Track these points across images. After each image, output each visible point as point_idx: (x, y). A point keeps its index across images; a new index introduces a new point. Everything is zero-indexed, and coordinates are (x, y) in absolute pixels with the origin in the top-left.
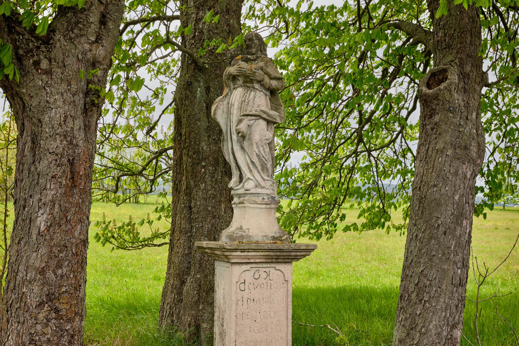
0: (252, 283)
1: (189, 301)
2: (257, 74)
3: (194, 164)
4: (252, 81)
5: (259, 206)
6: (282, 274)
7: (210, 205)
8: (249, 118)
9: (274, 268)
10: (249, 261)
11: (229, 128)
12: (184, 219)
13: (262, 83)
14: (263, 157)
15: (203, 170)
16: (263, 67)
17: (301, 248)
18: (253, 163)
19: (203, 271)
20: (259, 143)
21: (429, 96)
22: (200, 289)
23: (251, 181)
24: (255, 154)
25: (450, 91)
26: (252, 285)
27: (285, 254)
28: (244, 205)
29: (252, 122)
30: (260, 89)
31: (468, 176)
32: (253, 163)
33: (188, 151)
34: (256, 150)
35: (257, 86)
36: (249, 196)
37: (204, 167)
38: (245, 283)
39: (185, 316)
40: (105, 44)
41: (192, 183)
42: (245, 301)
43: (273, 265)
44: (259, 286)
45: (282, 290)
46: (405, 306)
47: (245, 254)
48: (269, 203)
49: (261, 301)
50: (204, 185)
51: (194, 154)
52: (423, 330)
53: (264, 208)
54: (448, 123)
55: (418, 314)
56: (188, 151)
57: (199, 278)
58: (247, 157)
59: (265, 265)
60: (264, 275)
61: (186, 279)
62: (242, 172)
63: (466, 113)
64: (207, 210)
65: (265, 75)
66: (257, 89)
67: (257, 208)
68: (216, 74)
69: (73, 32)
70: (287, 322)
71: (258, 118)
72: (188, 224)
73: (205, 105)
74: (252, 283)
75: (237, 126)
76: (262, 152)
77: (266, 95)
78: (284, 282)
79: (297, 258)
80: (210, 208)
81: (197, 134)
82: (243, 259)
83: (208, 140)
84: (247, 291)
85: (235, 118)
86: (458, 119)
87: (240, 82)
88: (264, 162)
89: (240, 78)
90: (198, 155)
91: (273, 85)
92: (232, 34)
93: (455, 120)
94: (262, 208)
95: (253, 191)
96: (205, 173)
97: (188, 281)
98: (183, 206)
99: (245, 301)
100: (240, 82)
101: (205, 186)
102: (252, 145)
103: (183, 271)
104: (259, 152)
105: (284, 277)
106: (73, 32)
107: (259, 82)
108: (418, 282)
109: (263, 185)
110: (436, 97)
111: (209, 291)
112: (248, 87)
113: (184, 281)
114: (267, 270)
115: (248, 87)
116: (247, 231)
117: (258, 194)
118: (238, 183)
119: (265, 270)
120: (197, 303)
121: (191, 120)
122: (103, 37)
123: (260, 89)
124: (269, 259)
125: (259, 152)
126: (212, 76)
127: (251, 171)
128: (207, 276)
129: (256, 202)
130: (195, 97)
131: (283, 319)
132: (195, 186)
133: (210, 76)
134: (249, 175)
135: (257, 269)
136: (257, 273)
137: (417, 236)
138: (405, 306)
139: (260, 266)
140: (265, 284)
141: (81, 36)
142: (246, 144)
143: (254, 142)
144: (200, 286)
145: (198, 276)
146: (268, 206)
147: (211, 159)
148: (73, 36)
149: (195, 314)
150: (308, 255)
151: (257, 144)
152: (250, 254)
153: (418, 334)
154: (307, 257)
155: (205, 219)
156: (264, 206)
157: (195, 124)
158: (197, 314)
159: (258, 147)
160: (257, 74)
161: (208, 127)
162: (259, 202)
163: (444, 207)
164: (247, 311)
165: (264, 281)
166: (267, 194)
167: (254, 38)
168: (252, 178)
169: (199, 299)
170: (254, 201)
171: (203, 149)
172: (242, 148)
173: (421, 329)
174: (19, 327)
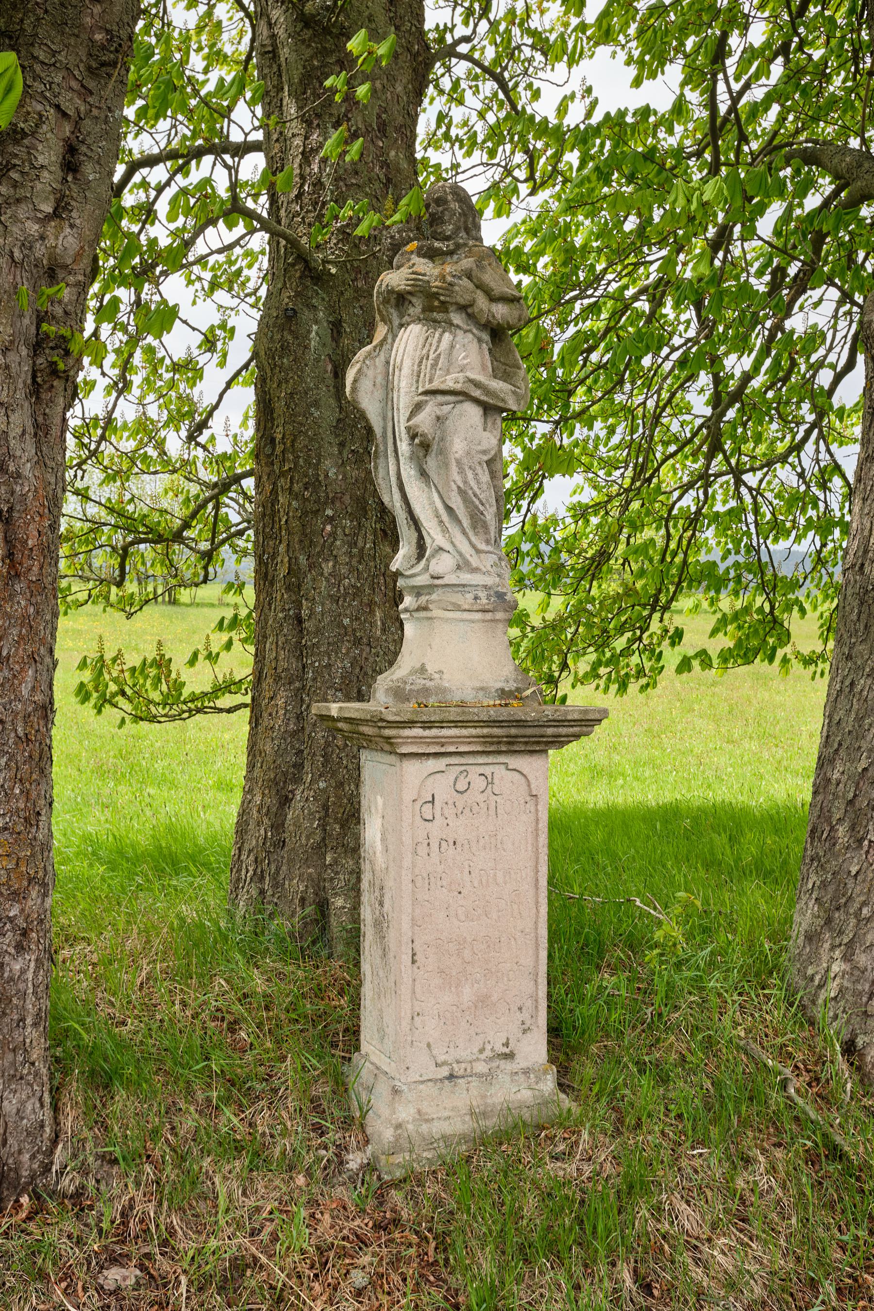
0: (450, 802)
1: (301, 846)
2: (457, 288)
3: (305, 513)
4: (444, 307)
5: (466, 615)
6: (523, 780)
7: (348, 612)
8: (440, 398)
9: (503, 767)
10: (443, 750)
12: (284, 648)
13: (470, 310)
14: (475, 495)
15: (328, 528)
16: (471, 270)
17: (569, 717)
19: (334, 774)
22: (327, 815)
23: (445, 555)
24: (454, 487)
26: (451, 806)
29: (447, 408)
30: (465, 327)
33: (292, 483)
35: (457, 318)
36: (440, 591)
37: (330, 519)
39: (291, 880)
40: (78, 221)
41: (302, 559)
43: (502, 759)
44: (467, 810)
45: (524, 818)
46: (821, 854)
47: (434, 732)
50: (331, 564)
51: (306, 489)
53: (478, 621)
55: (853, 873)
56: (292, 483)
57: (324, 790)
58: (435, 496)
59: (481, 760)
60: (481, 783)
61: (292, 792)
64: (340, 625)
65: (479, 292)
66: (458, 326)
67: (463, 620)
68: (357, 290)
71: (461, 398)
72: (293, 660)
73: (329, 367)
74: (450, 802)
76: (473, 483)
77: (480, 340)
78: (528, 798)
80: (346, 622)
81: (311, 440)
82: (429, 744)
83: (340, 453)
85: (404, 400)
87: (416, 309)
88: (477, 507)
90: (315, 491)
91: (499, 317)
92: (395, 186)
96: (333, 534)
97: (298, 797)
98: (281, 615)
101: (334, 566)
102: (447, 465)
103: (285, 774)
104: (465, 482)
105: (529, 786)
107: (463, 308)
108: (855, 796)
111: (347, 820)
112: (435, 321)
113: (287, 797)
114: (487, 770)
115: (435, 321)
116: (437, 676)
117: (464, 586)
119: (481, 770)
120: (320, 848)
121: (296, 405)
122: (73, 203)
123: (465, 327)
125: (465, 482)
126: (347, 295)
128: (342, 784)
129: (459, 606)
130: (306, 347)
131: (527, 887)
132: (311, 567)
133: (342, 293)
136: (462, 777)
137: (852, 684)
138: (821, 854)
139: (471, 760)
140: (482, 805)
141: (18, 201)
142: (431, 464)
144: (326, 808)
145: (322, 785)
146: (489, 616)
147: (347, 499)
149: (315, 876)
150: (587, 734)
151: (458, 462)
153: (853, 921)
155: (335, 646)
156: (478, 616)
157: (307, 414)
158: (319, 874)
159: (461, 471)
160: (457, 288)
161: (339, 421)
162: (467, 607)
164: (440, 869)
165: (481, 798)
166: (485, 587)
167: (450, 197)
168: (447, 546)
169: (324, 839)
170: (453, 604)
171: (327, 476)
172: (423, 474)
173: (860, 909)
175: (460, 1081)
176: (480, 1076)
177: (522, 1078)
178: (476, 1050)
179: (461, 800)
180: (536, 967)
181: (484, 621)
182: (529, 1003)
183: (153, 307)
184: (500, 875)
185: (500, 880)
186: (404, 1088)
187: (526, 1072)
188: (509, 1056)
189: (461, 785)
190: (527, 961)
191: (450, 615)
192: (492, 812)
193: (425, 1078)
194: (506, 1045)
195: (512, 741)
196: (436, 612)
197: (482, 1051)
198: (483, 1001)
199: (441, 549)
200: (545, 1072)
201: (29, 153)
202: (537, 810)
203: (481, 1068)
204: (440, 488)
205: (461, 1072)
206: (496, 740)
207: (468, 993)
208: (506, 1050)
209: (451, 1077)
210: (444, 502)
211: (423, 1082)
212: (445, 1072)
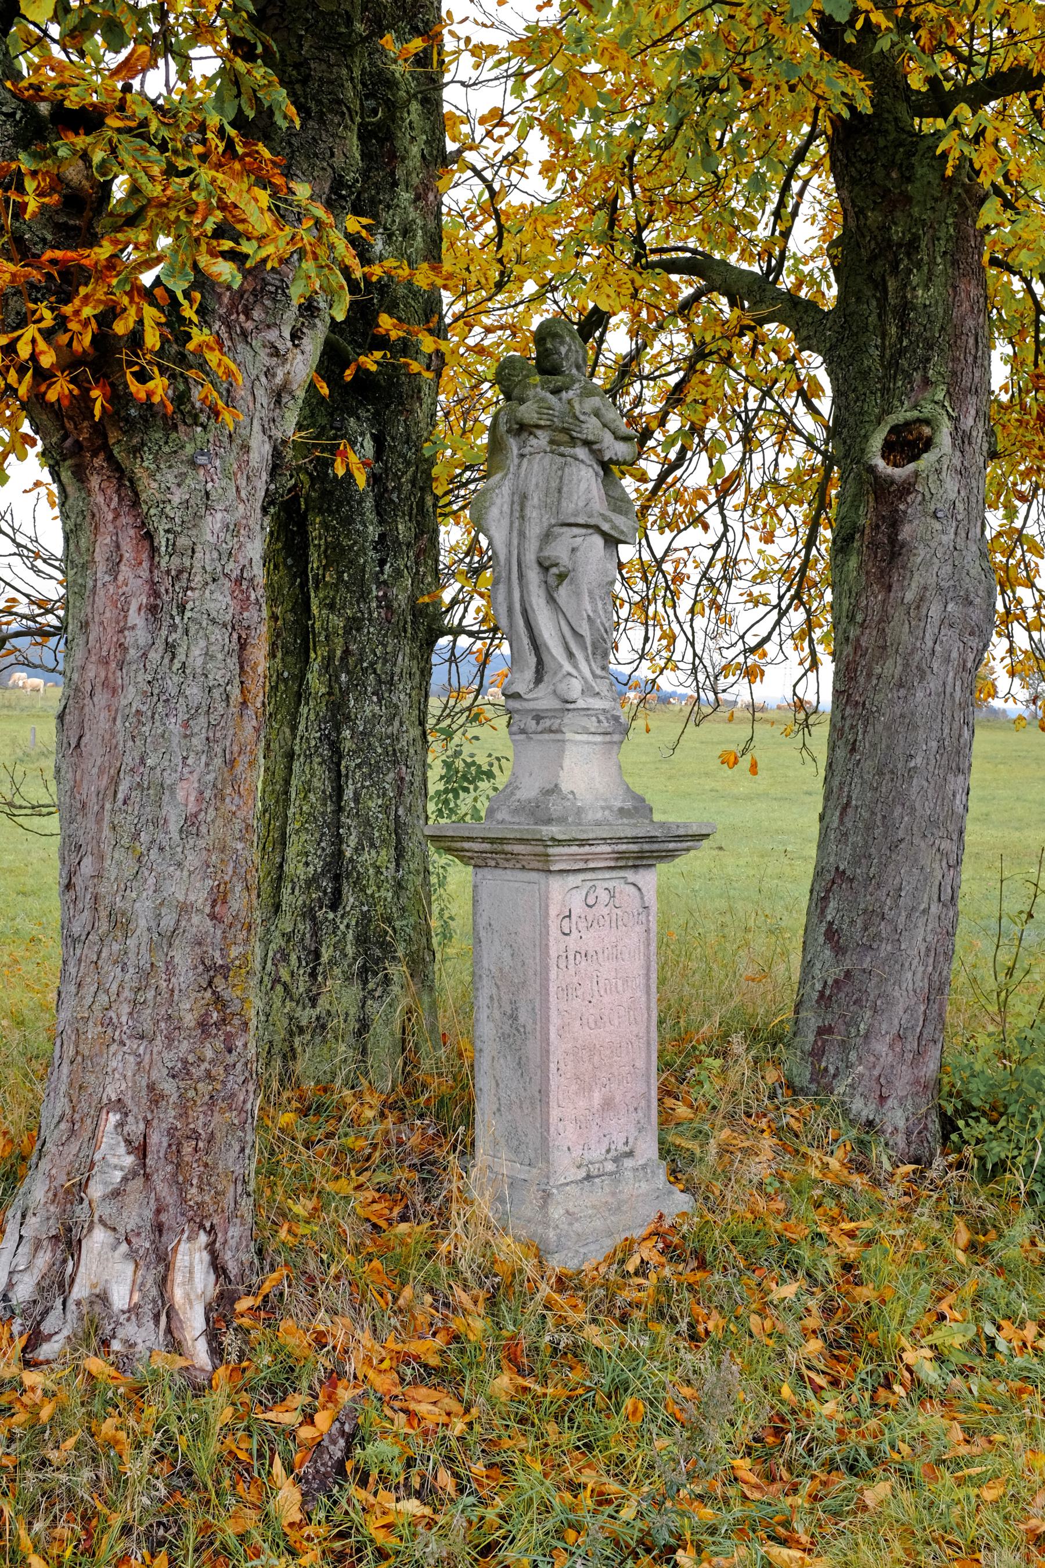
4: (573, 441)
5: (591, 738)
6: (637, 893)
8: (576, 531)
11: (515, 552)
13: (595, 447)
18: (575, 633)
20: (597, 591)
21: (892, 483)
25: (938, 472)
27: (655, 847)
28: (558, 736)
29: (579, 540)
30: (588, 462)
31: (969, 665)
32: (575, 633)
34: (589, 608)
35: (581, 452)
36: (570, 715)
38: (569, 916)
42: (571, 957)
44: (595, 924)
45: (638, 928)
47: (587, 849)
48: (609, 730)
49: (600, 955)
52: (879, 1003)
54: (933, 544)
58: (563, 623)
59: (607, 875)
60: (604, 896)
62: (545, 658)
63: (966, 522)
66: (582, 461)
67: (588, 743)
69: (248, 317)
70: (648, 1000)
71: (590, 531)
75: (541, 549)
77: (597, 474)
79: (669, 855)
82: (576, 861)
84: (575, 934)
85: (534, 531)
86: (952, 536)
89: (539, 432)
91: (619, 454)
93: (945, 539)
94: (595, 744)
95: (581, 704)
99: (571, 957)
100: (541, 440)
102: (578, 594)
105: (642, 898)
106: (248, 317)
107: (587, 443)
109: (597, 690)
110: (906, 488)
114: (610, 885)
116: (571, 796)
118: (532, 686)
119: (606, 885)
123: (588, 462)
124: (617, 859)
127: (571, 655)
131: (640, 995)
134: (567, 667)
135: (591, 883)
139: (600, 875)
141: (269, 327)
142: (563, 594)
143: (585, 588)
146: (608, 738)
148: (249, 325)
151: (590, 593)
152: (593, 849)
153: (869, 1013)
154: (692, 853)
156: (599, 738)
162: (593, 730)
163: (921, 731)
164: (575, 980)
165: (605, 911)
166: (604, 710)
170: (584, 727)
172: (551, 600)
174: (142, 1048)
175: (597, 1180)
176: (611, 1174)
177: (641, 1174)
178: (603, 1151)
179: (591, 913)
180: (648, 1069)
181: (605, 743)
182: (643, 1103)
183: (902, 507)
184: (620, 983)
185: (620, 989)
186: (555, 1191)
187: (644, 1167)
188: (630, 1154)
189: (591, 902)
190: (640, 1063)
191: (578, 737)
192: (614, 925)
193: (568, 1180)
194: (627, 1143)
195: (641, 855)
196: (569, 736)
197: (608, 1151)
198: (608, 1104)
199: (569, 674)
200: (659, 1168)
201: (282, 281)
202: (648, 921)
203: (610, 1167)
204: (568, 615)
205: (596, 1173)
206: (621, 856)
207: (597, 1097)
208: (627, 1149)
209: (588, 1177)
210: (572, 629)
211: (567, 1184)
212: (582, 1173)
